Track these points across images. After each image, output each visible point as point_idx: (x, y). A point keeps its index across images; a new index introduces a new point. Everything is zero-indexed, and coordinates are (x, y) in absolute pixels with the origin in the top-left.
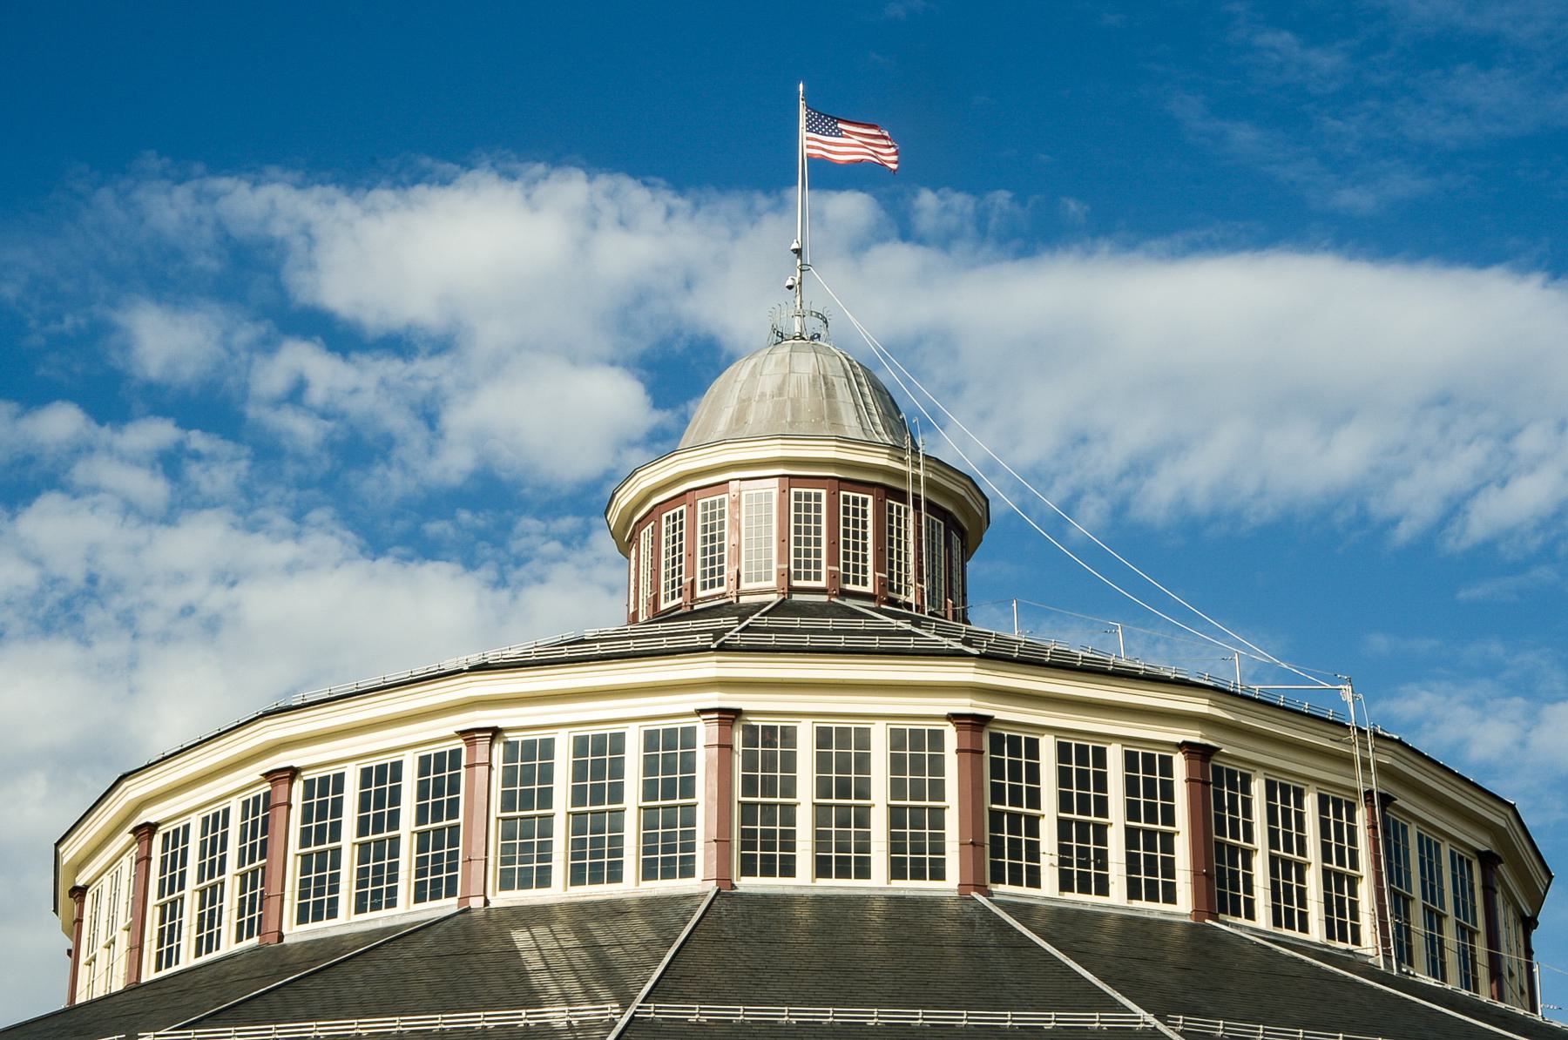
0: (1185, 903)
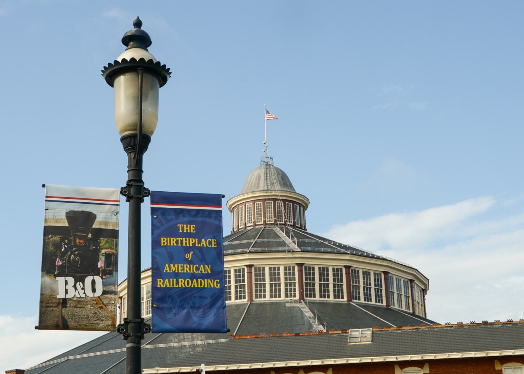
0: (345, 299)
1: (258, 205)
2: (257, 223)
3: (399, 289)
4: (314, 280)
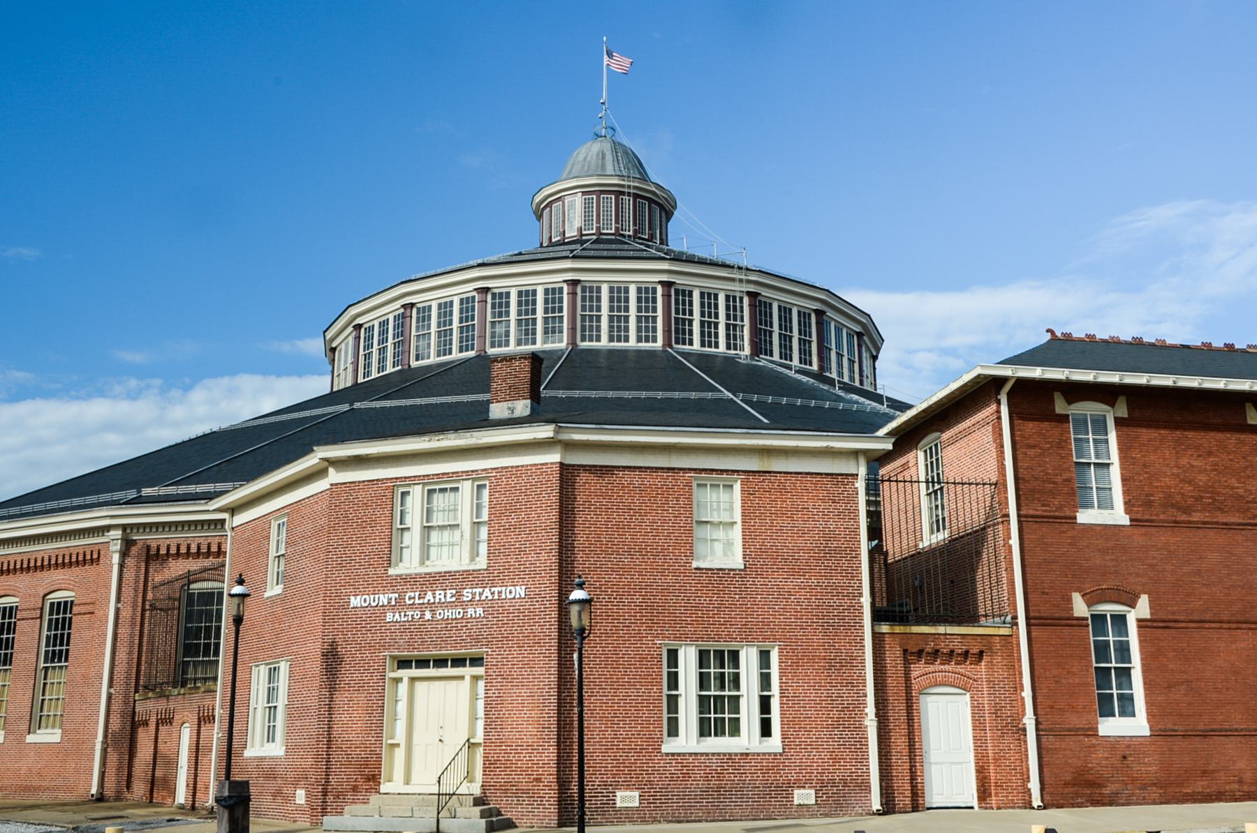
1: (587, 201)
2: (584, 232)
3: (839, 345)
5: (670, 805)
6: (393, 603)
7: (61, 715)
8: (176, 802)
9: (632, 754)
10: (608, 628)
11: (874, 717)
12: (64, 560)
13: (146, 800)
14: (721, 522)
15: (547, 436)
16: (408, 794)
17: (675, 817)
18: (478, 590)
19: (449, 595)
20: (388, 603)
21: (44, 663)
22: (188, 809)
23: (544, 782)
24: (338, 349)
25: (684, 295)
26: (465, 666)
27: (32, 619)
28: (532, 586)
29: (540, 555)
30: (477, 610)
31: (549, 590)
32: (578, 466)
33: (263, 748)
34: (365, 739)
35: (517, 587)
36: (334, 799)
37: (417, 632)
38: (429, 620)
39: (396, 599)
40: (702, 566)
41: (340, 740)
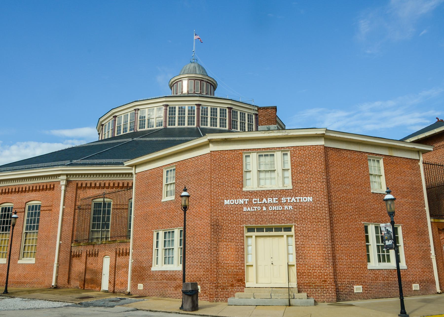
4: (216, 116)
5: (348, 289)
6: (246, 203)
7: (34, 252)
8: (101, 290)
9: (358, 270)
10: (345, 216)
11: (434, 255)
12: (5, 191)
13: (81, 288)
14: (376, 175)
15: (322, 133)
16: (260, 288)
17: (374, 296)
18: (289, 198)
19: (274, 200)
20: (244, 203)
21: (26, 230)
22: (111, 293)
23: (328, 282)
24: (105, 125)
25: (235, 112)
26: (282, 231)
27: (20, 212)
28: (315, 197)
29: (318, 184)
30: (289, 206)
31: (324, 199)
32: (328, 147)
33: (162, 267)
34: (236, 263)
35: (308, 197)
36: (221, 290)
37: (259, 216)
38: (265, 211)
39: (247, 201)
40: (374, 192)
41: (223, 263)
